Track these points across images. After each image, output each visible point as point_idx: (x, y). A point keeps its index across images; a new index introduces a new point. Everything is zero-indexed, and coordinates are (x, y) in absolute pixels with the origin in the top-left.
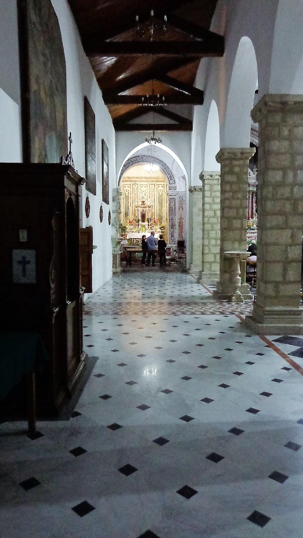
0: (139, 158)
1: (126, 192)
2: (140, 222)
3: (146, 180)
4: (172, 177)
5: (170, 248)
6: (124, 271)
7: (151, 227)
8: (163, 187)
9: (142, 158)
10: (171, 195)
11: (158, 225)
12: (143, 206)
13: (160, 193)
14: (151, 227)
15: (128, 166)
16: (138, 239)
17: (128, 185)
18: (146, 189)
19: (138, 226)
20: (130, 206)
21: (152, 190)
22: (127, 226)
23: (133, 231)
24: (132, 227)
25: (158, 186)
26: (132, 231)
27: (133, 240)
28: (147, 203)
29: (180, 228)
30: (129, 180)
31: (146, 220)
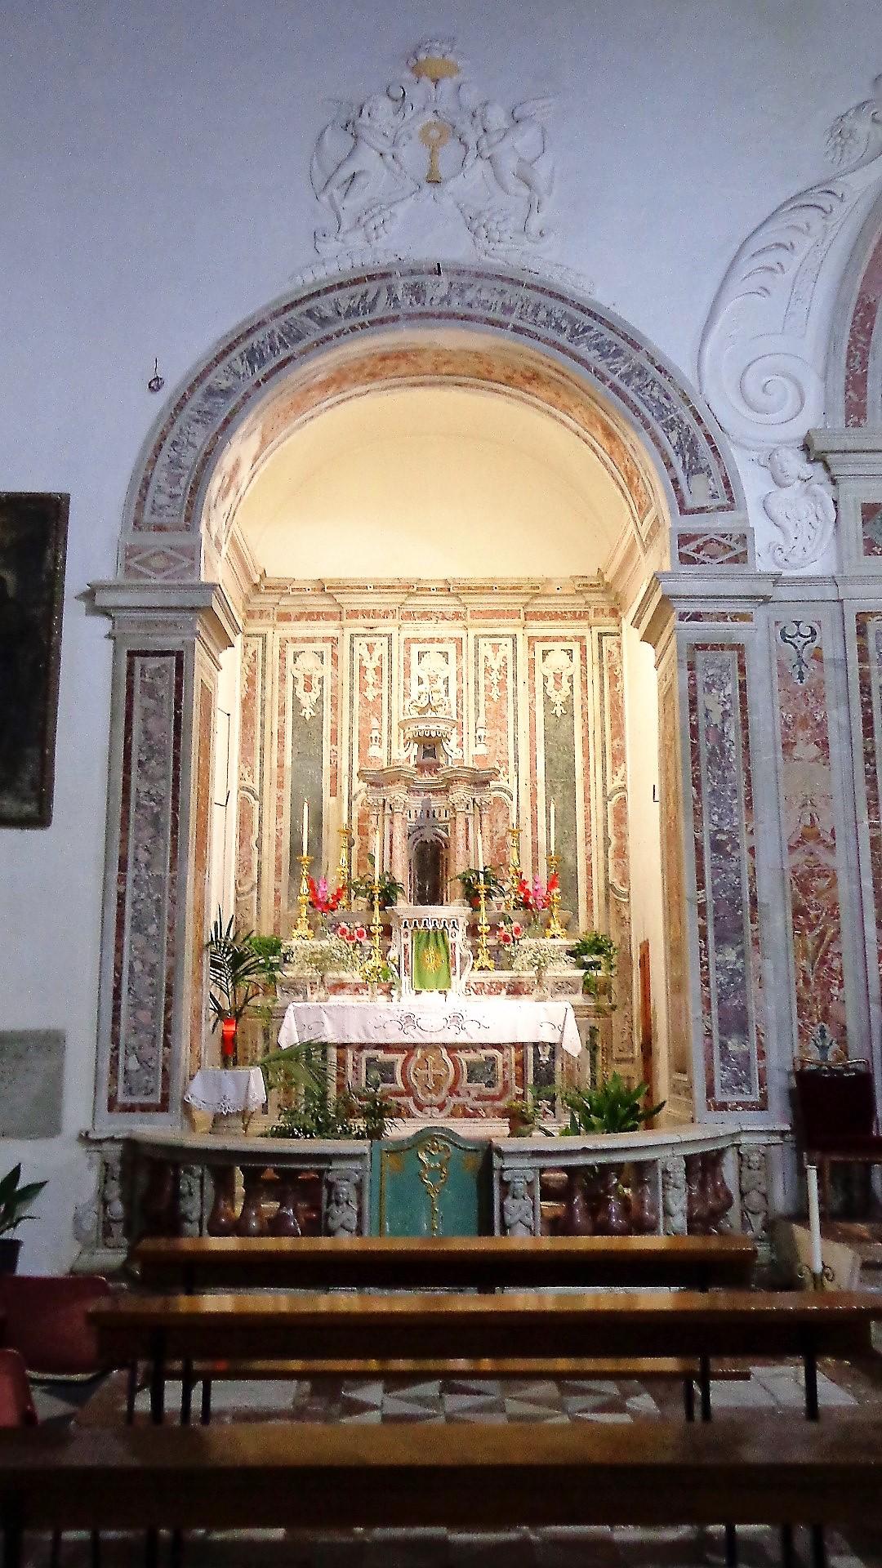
0: (389, 288)
2: (403, 906)
3: (449, 604)
4: (703, 445)
5: (721, 1153)
7: (492, 942)
8: (577, 654)
9: (417, 291)
10: (697, 617)
11: (556, 928)
12: (426, 778)
13: (558, 698)
15: (284, 354)
16: (386, 1048)
17: (319, 646)
18: (451, 671)
19: (387, 932)
20: (333, 793)
22: (295, 942)
23: (346, 976)
24: (330, 942)
25: (540, 647)
26: (332, 976)
27: (341, 1062)
28: (461, 752)
29: (811, 937)
30: (322, 604)
31: (453, 887)
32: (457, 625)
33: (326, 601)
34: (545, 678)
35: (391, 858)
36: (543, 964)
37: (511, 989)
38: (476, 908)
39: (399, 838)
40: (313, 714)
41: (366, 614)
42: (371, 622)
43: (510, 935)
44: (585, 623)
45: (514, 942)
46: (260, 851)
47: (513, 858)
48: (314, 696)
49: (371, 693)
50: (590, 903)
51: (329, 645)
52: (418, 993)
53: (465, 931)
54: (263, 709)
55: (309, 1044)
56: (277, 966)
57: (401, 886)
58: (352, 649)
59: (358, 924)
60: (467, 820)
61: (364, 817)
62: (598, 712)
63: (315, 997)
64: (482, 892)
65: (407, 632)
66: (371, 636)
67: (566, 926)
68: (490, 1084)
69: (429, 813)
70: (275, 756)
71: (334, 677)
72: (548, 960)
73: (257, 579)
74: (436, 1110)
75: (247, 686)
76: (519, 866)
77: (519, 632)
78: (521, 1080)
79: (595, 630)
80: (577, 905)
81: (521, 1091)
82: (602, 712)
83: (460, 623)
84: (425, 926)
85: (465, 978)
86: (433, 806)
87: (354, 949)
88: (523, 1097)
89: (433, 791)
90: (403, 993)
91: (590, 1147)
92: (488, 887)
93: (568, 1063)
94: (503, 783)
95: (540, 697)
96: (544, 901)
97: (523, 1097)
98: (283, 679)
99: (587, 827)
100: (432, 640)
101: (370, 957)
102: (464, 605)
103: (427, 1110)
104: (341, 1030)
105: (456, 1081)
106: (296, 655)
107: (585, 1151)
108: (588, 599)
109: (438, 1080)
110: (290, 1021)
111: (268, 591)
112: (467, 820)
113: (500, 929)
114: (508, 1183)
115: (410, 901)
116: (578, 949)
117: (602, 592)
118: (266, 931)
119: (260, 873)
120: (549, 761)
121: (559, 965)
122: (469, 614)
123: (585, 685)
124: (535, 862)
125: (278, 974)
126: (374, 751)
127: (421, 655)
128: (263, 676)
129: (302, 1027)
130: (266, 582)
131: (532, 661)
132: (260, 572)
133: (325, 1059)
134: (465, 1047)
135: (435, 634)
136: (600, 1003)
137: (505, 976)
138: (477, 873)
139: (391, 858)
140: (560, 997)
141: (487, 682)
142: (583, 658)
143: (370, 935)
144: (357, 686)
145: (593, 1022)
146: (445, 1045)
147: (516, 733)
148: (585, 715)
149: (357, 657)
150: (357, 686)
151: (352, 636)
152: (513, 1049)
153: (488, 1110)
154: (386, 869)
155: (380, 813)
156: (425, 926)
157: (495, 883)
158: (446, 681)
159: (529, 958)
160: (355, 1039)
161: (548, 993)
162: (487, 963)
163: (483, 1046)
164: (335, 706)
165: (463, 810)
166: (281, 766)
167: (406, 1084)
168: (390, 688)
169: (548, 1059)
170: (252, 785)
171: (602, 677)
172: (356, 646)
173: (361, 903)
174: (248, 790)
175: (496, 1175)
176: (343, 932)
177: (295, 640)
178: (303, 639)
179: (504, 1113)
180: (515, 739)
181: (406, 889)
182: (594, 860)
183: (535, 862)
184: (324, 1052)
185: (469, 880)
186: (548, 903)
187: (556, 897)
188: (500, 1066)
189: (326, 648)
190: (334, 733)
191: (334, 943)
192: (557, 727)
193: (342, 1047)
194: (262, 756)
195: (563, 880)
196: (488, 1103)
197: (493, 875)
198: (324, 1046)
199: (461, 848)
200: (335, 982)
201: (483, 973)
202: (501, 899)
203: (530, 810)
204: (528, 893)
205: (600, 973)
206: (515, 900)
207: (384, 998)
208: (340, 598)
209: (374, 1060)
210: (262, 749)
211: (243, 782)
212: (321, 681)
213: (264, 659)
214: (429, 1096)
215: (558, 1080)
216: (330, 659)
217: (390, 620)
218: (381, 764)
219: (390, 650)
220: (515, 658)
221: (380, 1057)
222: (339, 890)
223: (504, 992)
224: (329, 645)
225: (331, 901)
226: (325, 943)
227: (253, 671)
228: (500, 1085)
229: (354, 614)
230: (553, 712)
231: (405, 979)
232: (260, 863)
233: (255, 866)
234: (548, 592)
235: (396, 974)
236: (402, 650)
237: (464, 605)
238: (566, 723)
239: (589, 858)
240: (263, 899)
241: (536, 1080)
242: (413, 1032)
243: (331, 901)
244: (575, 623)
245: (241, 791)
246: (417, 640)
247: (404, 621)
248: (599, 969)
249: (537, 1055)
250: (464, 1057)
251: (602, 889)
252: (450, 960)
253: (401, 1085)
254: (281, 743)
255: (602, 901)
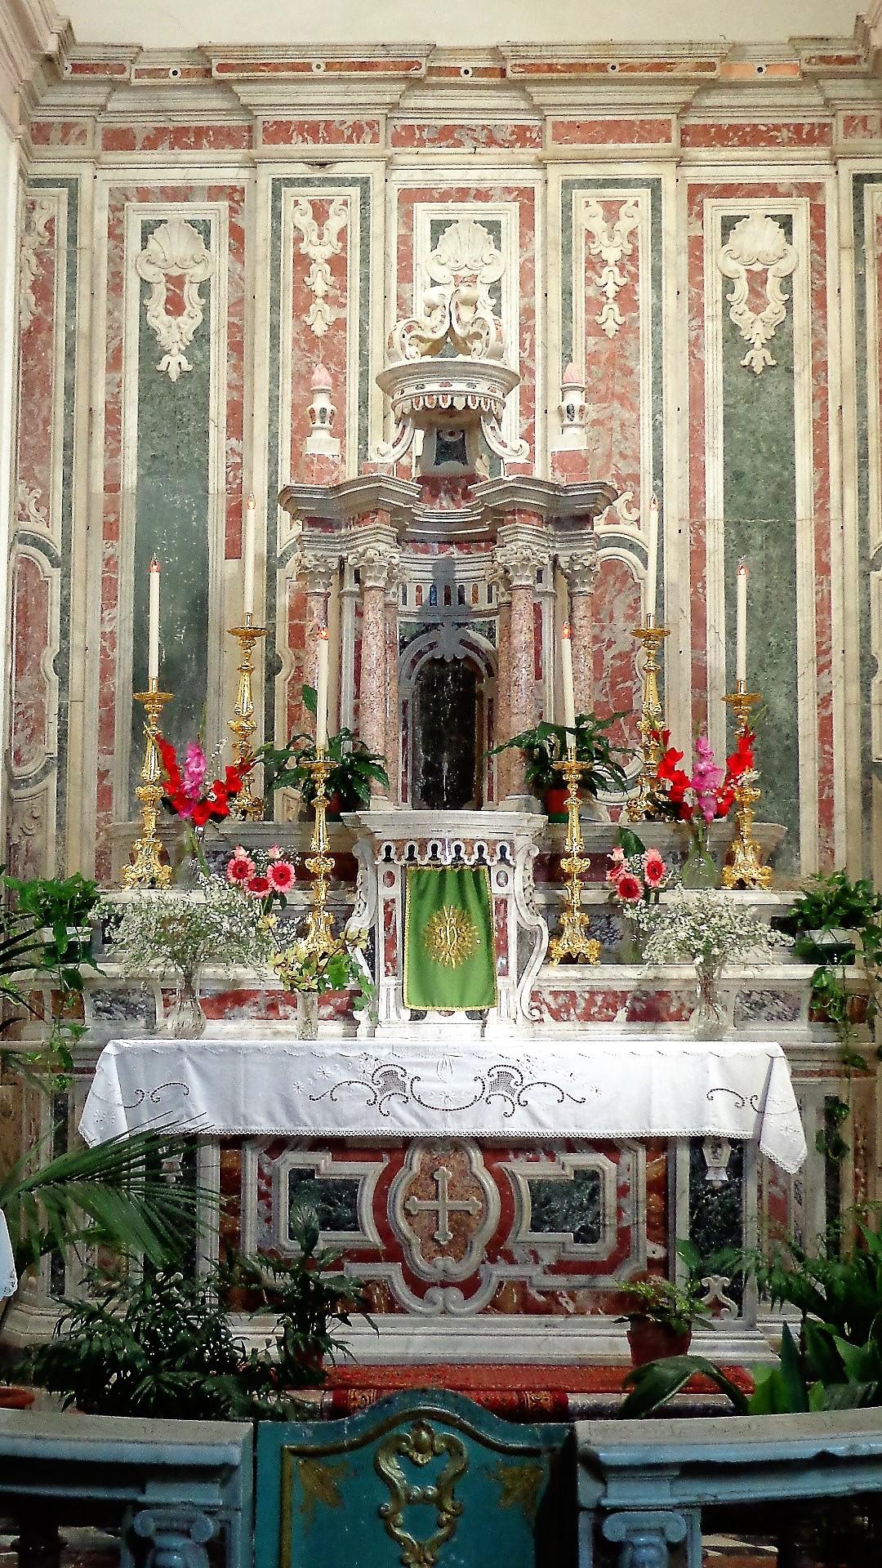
1: (159, 319)
6: (466, 1298)
7: (595, 895)
11: (747, 862)
12: (445, 508)
13: (757, 330)
14: (595, 895)
16: (339, 1146)
17: (199, 208)
18: (506, 264)
19: (346, 870)
21: (611, 279)
22: (128, 895)
23: (245, 974)
25: (715, 210)
27: (231, 1182)
30: (207, 106)
32: (523, 158)
33: (215, 101)
34: (728, 284)
35: (357, 696)
36: (716, 951)
37: (639, 1006)
38: (555, 812)
39: (374, 650)
40: (186, 367)
41: (311, 131)
42: (322, 150)
43: (637, 879)
44: (822, 152)
45: (646, 897)
46: (64, 683)
47: (647, 699)
48: (188, 324)
49: (320, 320)
50: (826, 808)
51: (224, 205)
52: (417, 1016)
53: (530, 866)
54: (70, 354)
55: (152, 1138)
56: (83, 952)
57: (378, 762)
58: (277, 215)
59: (276, 853)
60: (537, 611)
61: (298, 610)
62: (850, 361)
63: (171, 1024)
64: (572, 778)
65: (404, 175)
66: (324, 182)
67: (770, 858)
68: (587, 1235)
69: (449, 594)
70: (99, 466)
71: (236, 281)
72: (729, 940)
73: (51, 46)
74: (455, 1294)
75: (33, 299)
76: (662, 716)
77: (667, 174)
78: (661, 1227)
79: (848, 168)
80: (796, 810)
81: (659, 1253)
82: (861, 362)
83: (528, 154)
84: (434, 857)
85: (528, 983)
86: (458, 575)
87: (267, 911)
88: (663, 1266)
89: (463, 543)
90: (382, 1016)
91: (839, 1449)
92: (585, 765)
93: (773, 1182)
94: (626, 529)
95: (713, 328)
96: (720, 800)
97: (663, 1266)
98: (116, 286)
99: (822, 629)
100: (462, 194)
101: (303, 932)
102: (537, 109)
103: (436, 1294)
104: (232, 1110)
105: (505, 1225)
106: (147, 230)
107: (825, 1462)
108: (831, 93)
109: (461, 1223)
110: (108, 1077)
111: (78, 76)
112: (537, 611)
113: (613, 866)
114: (618, 1548)
115: (405, 800)
116: (800, 915)
117: (865, 76)
118: (81, 863)
119: (63, 735)
120: (734, 477)
121: (757, 953)
122: (549, 132)
123: (819, 299)
124: (700, 712)
125: (84, 969)
126: (320, 443)
127: (438, 228)
128: (72, 278)
129: (134, 1100)
130: (76, 53)
131: (696, 246)
132: (58, 27)
133: (190, 1178)
134: (526, 1146)
135: (470, 179)
136: (852, 1043)
137: (626, 976)
138: (561, 732)
139: (357, 696)
140: (757, 1027)
141: (591, 292)
142: (818, 236)
143: (305, 877)
144: (287, 301)
145: (833, 1087)
146: (481, 1142)
147: (658, 411)
148: (820, 369)
149: (287, 232)
150: (287, 301)
151: (278, 185)
152: (642, 1154)
153: (581, 1294)
154: (347, 723)
155: (332, 589)
156: (434, 857)
157: (603, 757)
158: (495, 289)
159: (682, 935)
160: (262, 1125)
161: (726, 1018)
162: (582, 946)
163: (571, 1145)
164: (236, 348)
165: (530, 582)
166: (112, 487)
167: (385, 1232)
168: (365, 304)
169: (725, 1178)
170: (45, 530)
171: (860, 279)
172: (287, 206)
173: (287, 800)
174: (37, 543)
175: (584, 1522)
176: (241, 871)
177: (144, 195)
178: (163, 190)
179: (623, 1304)
180: (657, 428)
181: (397, 771)
182: (837, 707)
183: (700, 712)
184: (191, 1159)
185: (543, 750)
186: (728, 805)
187: (748, 790)
188: (609, 1195)
189: (217, 212)
190: (235, 410)
191: (216, 897)
192: (751, 398)
193: (232, 1143)
194: (68, 462)
195: (767, 753)
196: (582, 1279)
197: (600, 739)
198: (192, 1141)
199: (523, 673)
200: (220, 988)
201: (572, 972)
202: (617, 796)
203: (689, 591)
204: (680, 780)
205: (852, 973)
206: (650, 797)
207: (337, 1027)
208: (248, 94)
209: (310, 1174)
210: (68, 446)
211: (24, 524)
212: (204, 289)
213: (72, 238)
214: (440, 1261)
215: (752, 1232)
216: (226, 240)
217: (365, 147)
218: (335, 475)
219: (365, 219)
220: (657, 235)
221: (322, 1167)
222: (231, 771)
223: (622, 1014)
224: (224, 205)
225: (213, 797)
226: (197, 897)
227: (45, 263)
228: (610, 1238)
229: (280, 132)
230: (745, 362)
231: (387, 983)
232: (63, 713)
233: (54, 719)
234: (734, 77)
235: (366, 971)
236: (394, 216)
237: (537, 109)
238: (775, 387)
239: (825, 702)
240: (72, 790)
241: (695, 1225)
242: (400, 1110)
243: (213, 797)
244: (798, 153)
245: (20, 547)
246: (424, 195)
247: (397, 150)
248: (851, 961)
249: (698, 1168)
250: (523, 1170)
251: (855, 772)
252: (494, 943)
253: (372, 1236)
254: (114, 434)
255: (856, 804)
